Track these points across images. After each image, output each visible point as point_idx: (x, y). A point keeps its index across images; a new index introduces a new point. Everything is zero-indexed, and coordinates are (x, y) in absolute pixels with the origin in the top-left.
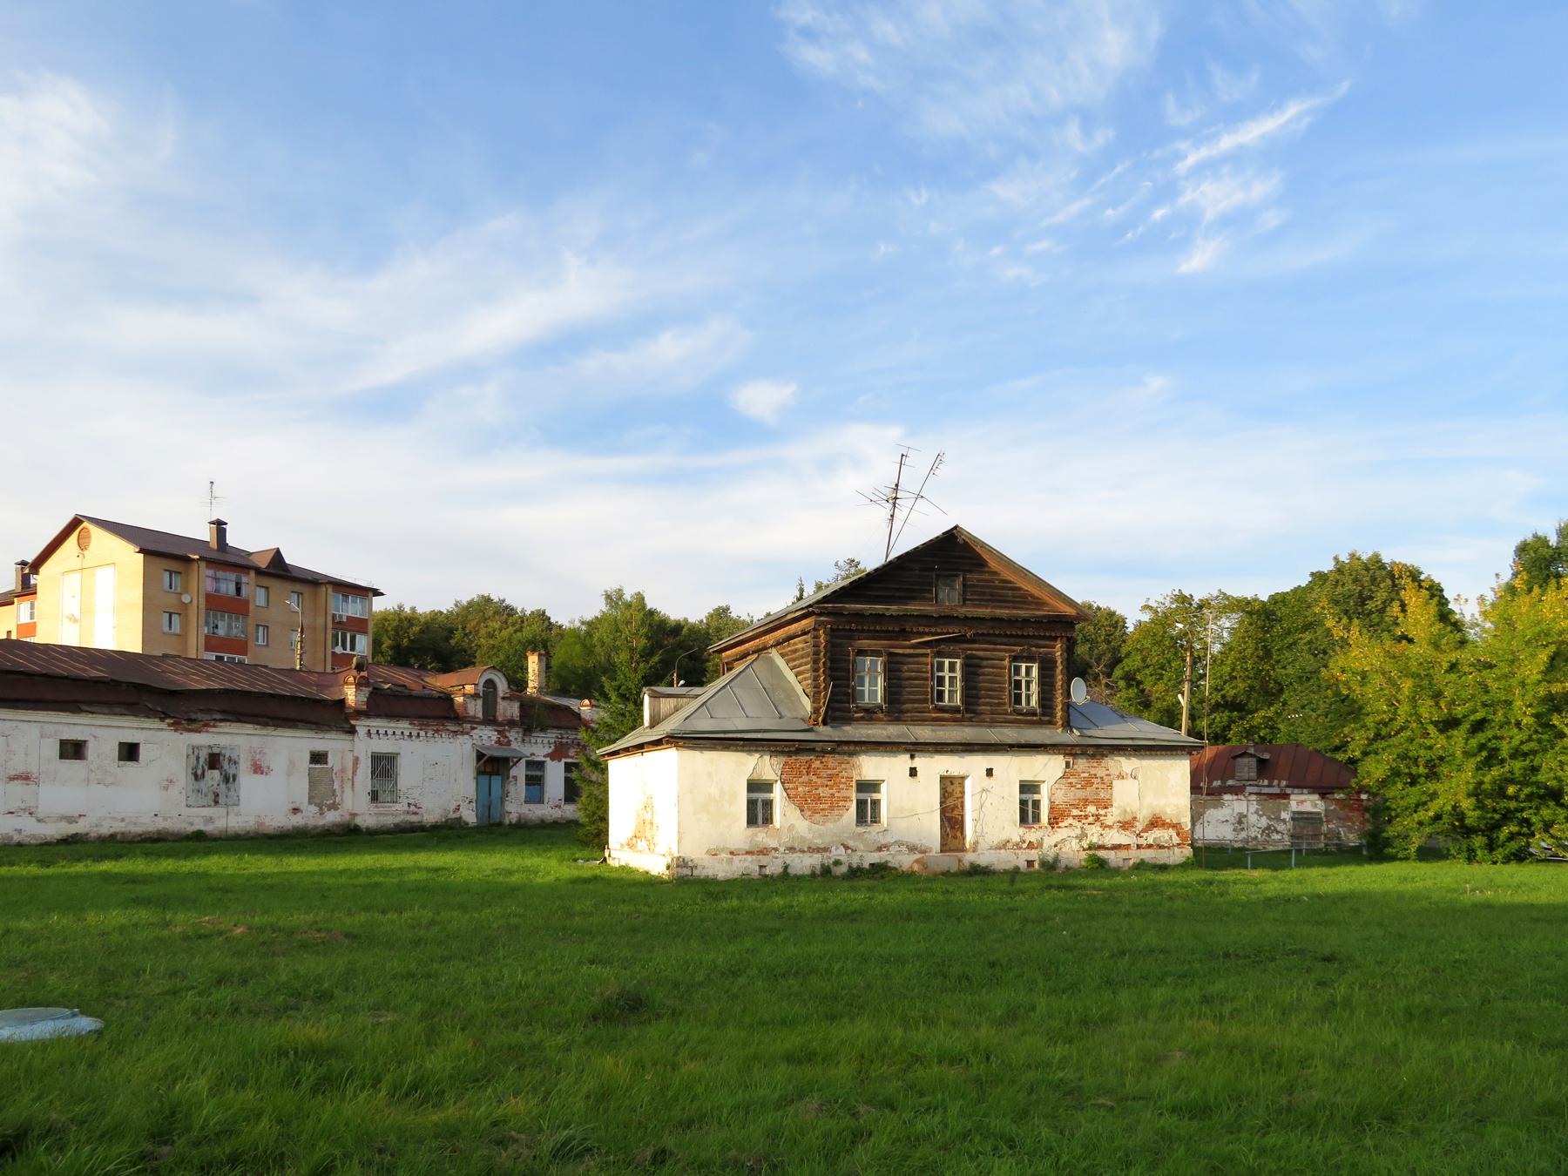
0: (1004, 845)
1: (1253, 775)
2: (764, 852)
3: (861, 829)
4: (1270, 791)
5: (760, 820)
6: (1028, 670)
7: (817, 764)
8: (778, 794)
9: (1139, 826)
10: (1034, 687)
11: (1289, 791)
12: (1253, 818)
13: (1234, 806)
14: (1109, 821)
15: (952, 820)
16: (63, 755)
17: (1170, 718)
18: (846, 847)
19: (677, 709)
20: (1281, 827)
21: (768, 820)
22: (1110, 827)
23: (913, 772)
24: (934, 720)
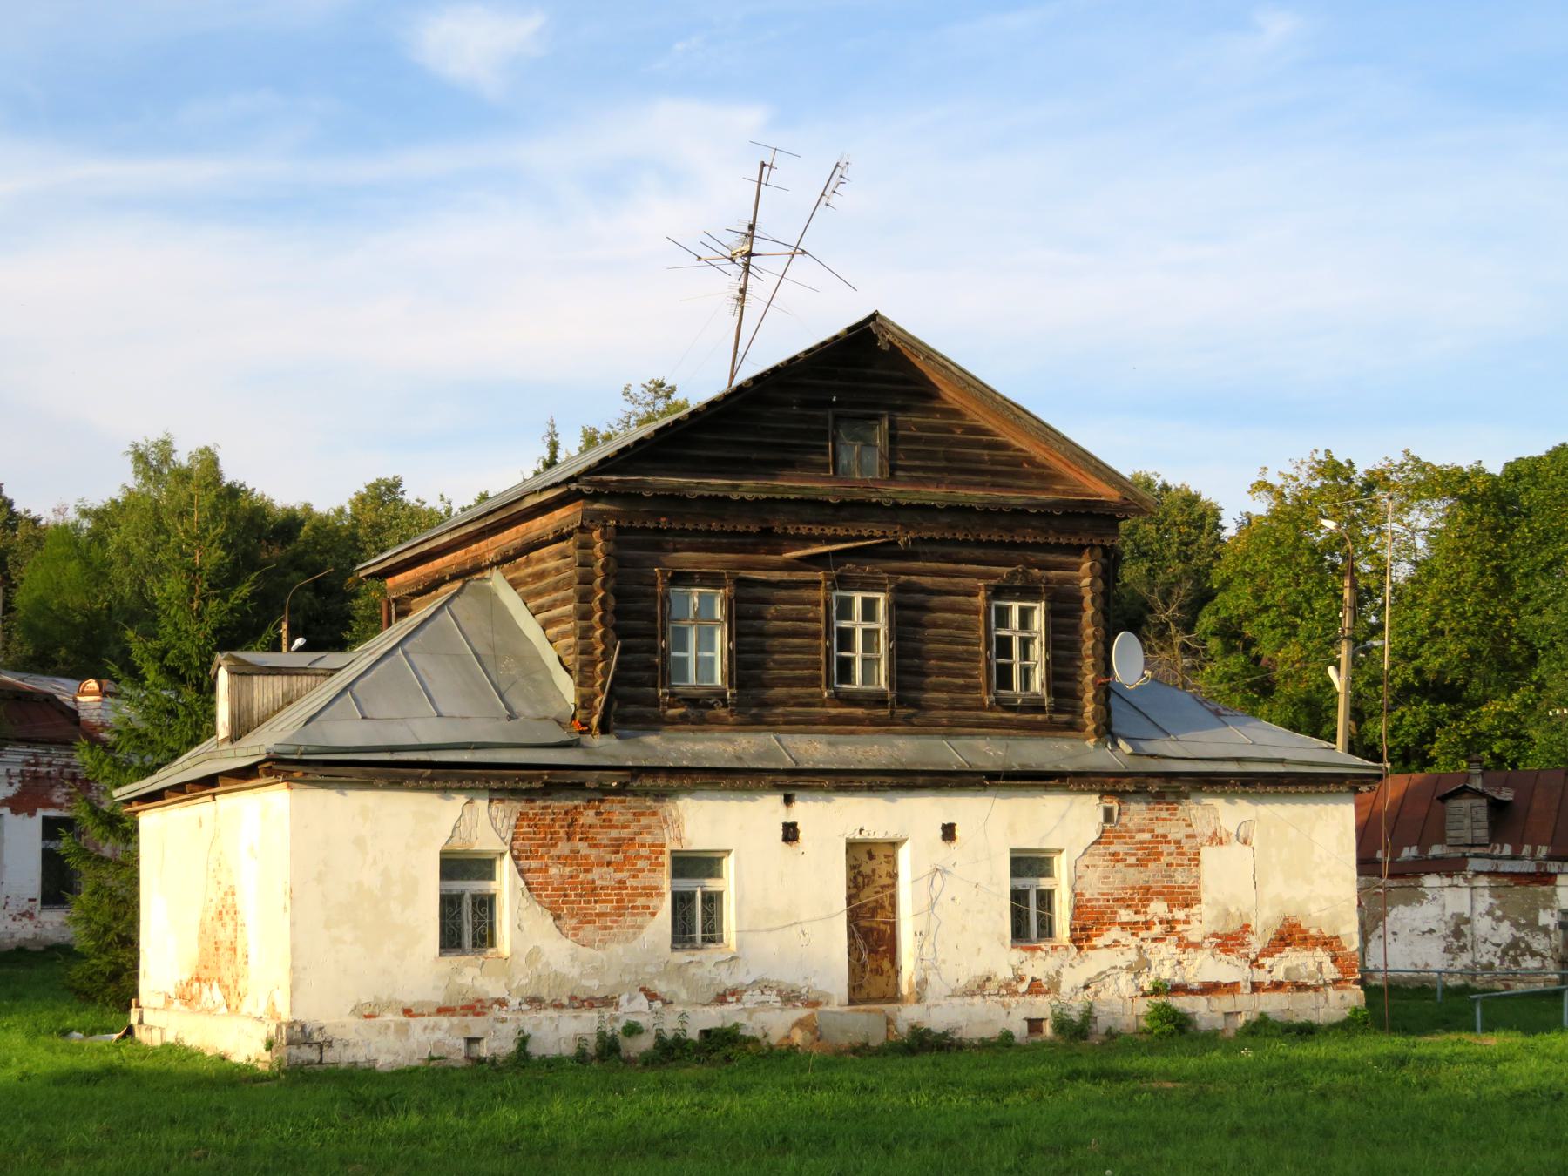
0: (980, 987)
1: (1482, 834)
3: (682, 957)
4: (1516, 867)
5: (467, 939)
6: (1025, 615)
7: (588, 817)
8: (505, 883)
9: (1256, 944)
10: (1038, 651)
11: (1553, 867)
12: (1483, 925)
13: (1444, 898)
14: (1194, 933)
15: (872, 934)
17: (1312, 716)
18: (652, 996)
19: (288, 701)
20: (1539, 943)
21: (485, 938)
22: (1197, 946)
23: (790, 833)
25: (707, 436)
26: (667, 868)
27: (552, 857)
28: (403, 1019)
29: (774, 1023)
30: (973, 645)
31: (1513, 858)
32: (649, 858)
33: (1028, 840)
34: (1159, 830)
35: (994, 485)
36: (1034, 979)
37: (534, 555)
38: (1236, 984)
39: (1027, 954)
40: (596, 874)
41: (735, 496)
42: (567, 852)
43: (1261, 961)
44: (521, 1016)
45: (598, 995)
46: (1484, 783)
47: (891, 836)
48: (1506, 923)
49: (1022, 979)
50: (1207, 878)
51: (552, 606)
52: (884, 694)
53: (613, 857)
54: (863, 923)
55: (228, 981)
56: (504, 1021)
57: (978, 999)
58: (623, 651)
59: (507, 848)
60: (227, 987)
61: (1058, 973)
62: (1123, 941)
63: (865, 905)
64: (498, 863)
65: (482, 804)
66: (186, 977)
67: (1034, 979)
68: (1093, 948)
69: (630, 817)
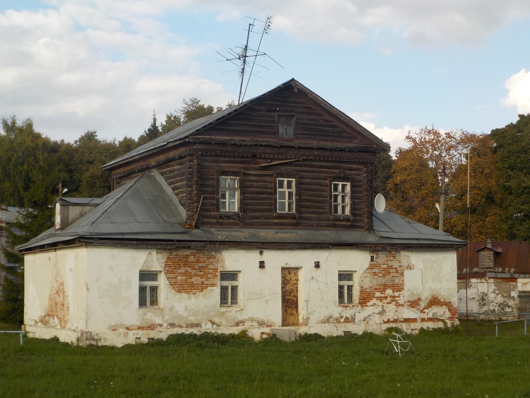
0: (327, 320)
1: (491, 264)
2: (151, 327)
3: (223, 309)
4: (503, 276)
5: (148, 303)
6: (344, 187)
7: (192, 259)
8: (162, 282)
9: (423, 305)
10: (348, 200)
11: (516, 276)
12: (492, 296)
13: (480, 287)
14: (401, 302)
15: (289, 302)
16: (260, 262)
17: (432, 221)
18: (213, 323)
19: (82, 215)
20: (511, 303)
21: (154, 302)
22: (402, 305)
23: (262, 265)
24: (276, 224)
25: (233, 122)
26: (219, 277)
27: (179, 273)
28: (126, 331)
29: (256, 333)
30: (325, 197)
31: (502, 272)
32: (212, 274)
33: (345, 268)
34: (390, 264)
35: (333, 141)
36: (346, 317)
37: (171, 164)
38: (416, 319)
39: (344, 308)
40: (194, 279)
41: (243, 143)
42: (184, 271)
43: (424, 311)
44: (167, 330)
45: (195, 323)
46: (492, 246)
47: (297, 266)
48: (500, 295)
49: (342, 317)
50: (405, 282)
51: (177, 182)
52: (295, 215)
53: (200, 273)
54: (286, 297)
55: (61, 316)
56: (161, 332)
57: (327, 324)
58: (204, 199)
59: (163, 270)
60: (60, 318)
61: (354, 315)
62: (377, 304)
63: (287, 290)
64: (159, 275)
65: (154, 253)
66: (43, 314)
67: (346, 317)
68: (367, 306)
69: (206, 259)
